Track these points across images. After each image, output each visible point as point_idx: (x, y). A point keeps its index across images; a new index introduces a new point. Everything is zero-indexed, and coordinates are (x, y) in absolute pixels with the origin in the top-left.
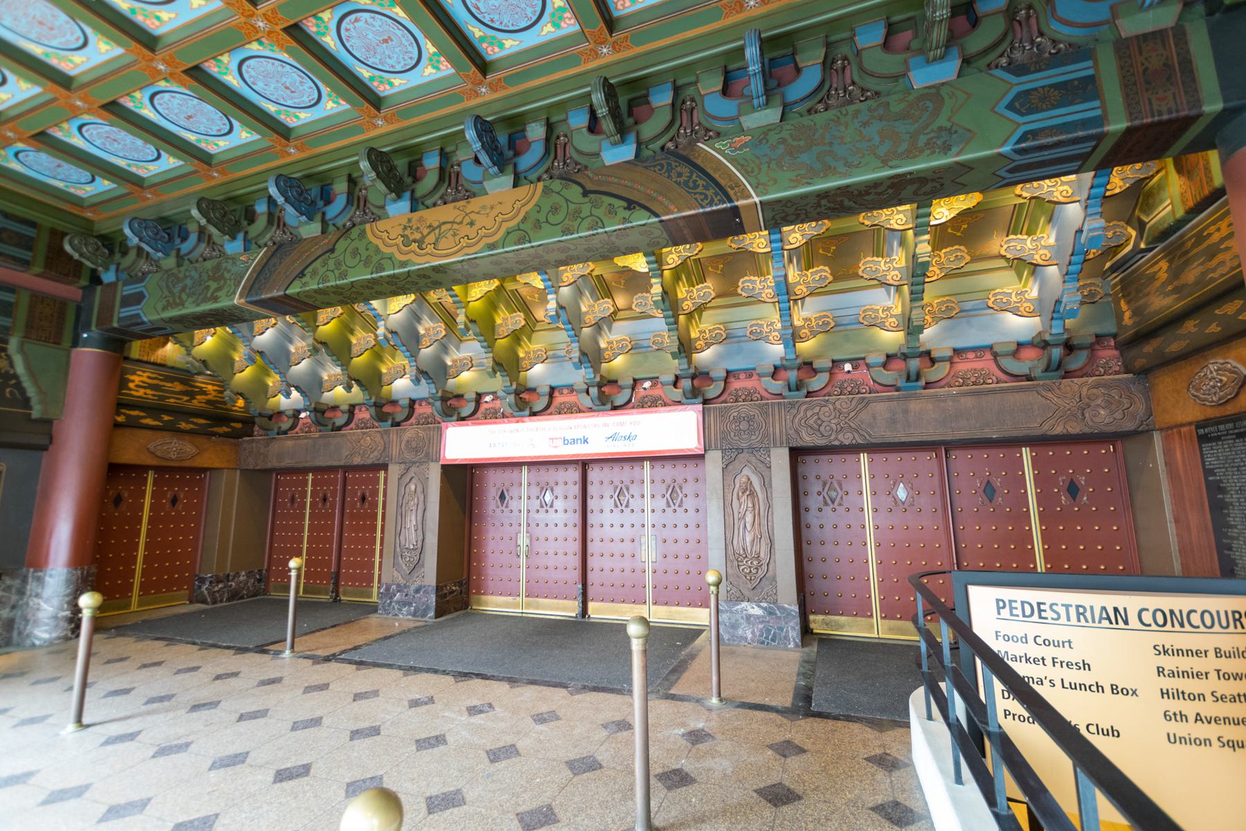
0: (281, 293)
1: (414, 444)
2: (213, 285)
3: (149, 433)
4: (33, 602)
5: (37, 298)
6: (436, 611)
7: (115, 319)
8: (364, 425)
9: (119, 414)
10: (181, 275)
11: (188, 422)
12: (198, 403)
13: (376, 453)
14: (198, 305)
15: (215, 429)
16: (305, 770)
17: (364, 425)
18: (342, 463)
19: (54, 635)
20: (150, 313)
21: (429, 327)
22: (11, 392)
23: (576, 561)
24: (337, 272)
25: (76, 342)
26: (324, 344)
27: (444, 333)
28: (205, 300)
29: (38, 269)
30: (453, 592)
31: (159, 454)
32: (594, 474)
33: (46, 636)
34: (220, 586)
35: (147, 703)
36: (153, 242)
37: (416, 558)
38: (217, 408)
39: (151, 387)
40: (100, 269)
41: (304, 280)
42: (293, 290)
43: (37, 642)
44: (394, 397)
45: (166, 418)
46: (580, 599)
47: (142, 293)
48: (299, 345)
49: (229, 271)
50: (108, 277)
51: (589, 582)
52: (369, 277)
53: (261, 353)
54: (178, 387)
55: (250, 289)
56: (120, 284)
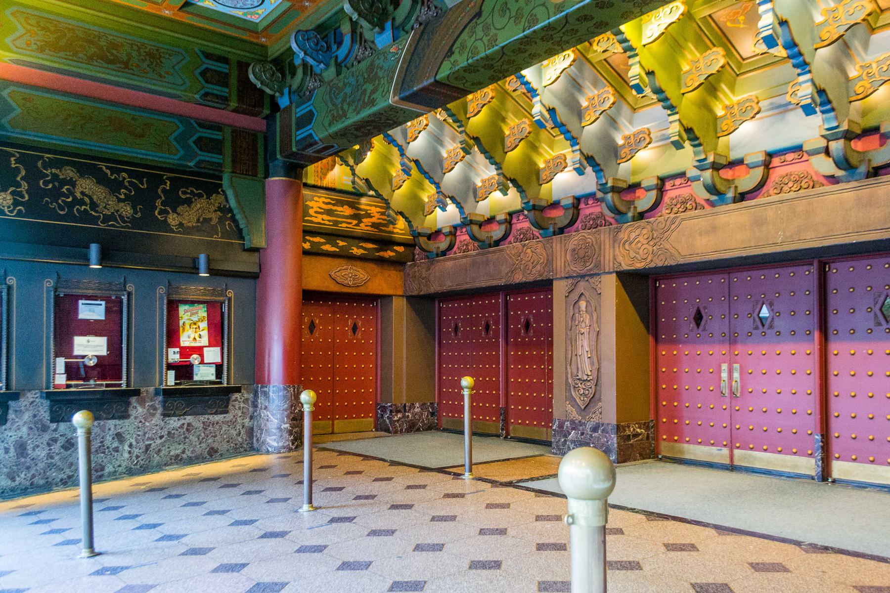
0: (432, 80)
1: (582, 253)
2: (369, 87)
3: (329, 260)
4: (264, 413)
5: (238, 133)
6: (619, 454)
7: (294, 144)
8: (525, 236)
9: (305, 241)
10: (341, 85)
12: (364, 227)
13: (538, 267)
14: (358, 113)
15: (381, 254)
16: (497, 565)
17: (525, 236)
18: (502, 282)
19: (281, 444)
20: (319, 131)
21: (596, 96)
23: (811, 405)
24: (485, 39)
25: (267, 176)
26: (476, 139)
27: (612, 100)
28: (365, 105)
29: (234, 104)
30: (636, 435)
31: (338, 280)
32: (838, 272)
33: (275, 444)
34: (399, 415)
35: (354, 499)
36: (314, 55)
37: (592, 391)
38: (381, 231)
39: (329, 212)
40: (277, 94)
41: (452, 59)
42: (444, 73)
43: (270, 449)
44: (555, 198)
45: (341, 243)
46: (819, 454)
47: (311, 111)
48: (450, 147)
49: (381, 68)
50: (284, 102)
51: (815, 296)
52: (521, 35)
53: (416, 162)
54: (347, 211)
55: (403, 83)
56: (294, 105)
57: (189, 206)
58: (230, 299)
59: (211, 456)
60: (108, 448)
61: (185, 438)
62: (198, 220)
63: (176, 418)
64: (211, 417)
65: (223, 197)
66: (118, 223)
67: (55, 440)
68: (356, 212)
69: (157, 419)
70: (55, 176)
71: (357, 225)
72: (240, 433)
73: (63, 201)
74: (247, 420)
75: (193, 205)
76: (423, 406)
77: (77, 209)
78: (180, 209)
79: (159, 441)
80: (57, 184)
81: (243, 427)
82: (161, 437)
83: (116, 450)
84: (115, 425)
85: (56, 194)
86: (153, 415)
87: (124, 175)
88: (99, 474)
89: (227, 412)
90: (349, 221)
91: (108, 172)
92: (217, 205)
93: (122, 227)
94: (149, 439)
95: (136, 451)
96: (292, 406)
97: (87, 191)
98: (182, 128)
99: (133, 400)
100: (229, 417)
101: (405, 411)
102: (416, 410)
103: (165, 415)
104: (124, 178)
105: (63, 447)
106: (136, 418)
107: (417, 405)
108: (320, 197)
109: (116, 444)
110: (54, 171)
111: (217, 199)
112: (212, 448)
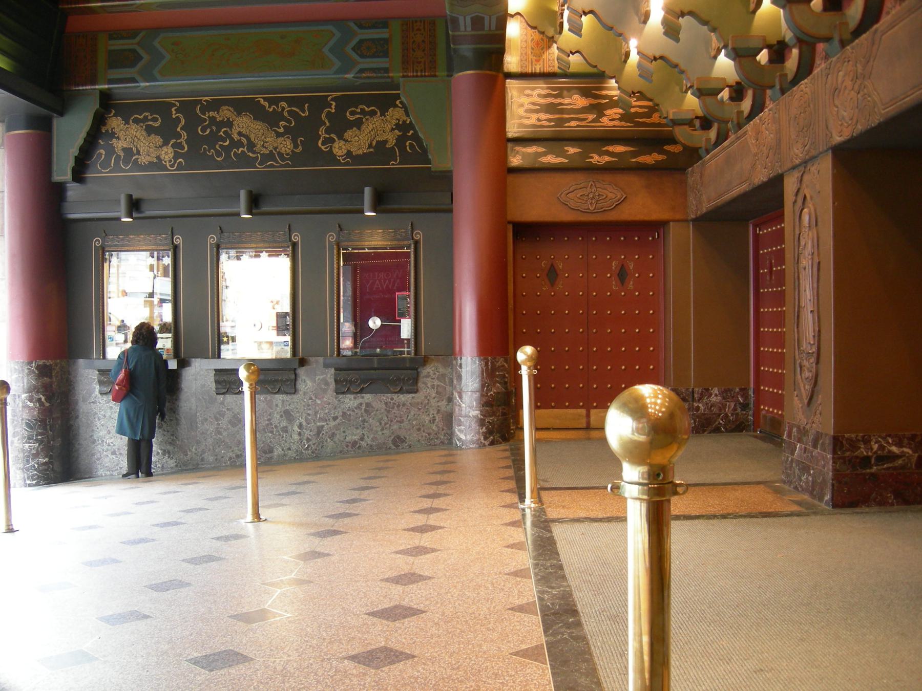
3: (558, 178)
11: (601, 154)
12: (611, 119)
22: (411, 145)
25: (450, 71)
31: (572, 204)
45: (572, 150)
54: (579, 101)
57: (359, 129)
58: (417, 243)
59: (397, 446)
60: (276, 426)
61: (364, 421)
62: (370, 146)
63: (352, 396)
64: (395, 396)
65: (402, 111)
66: (277, 162)
67: (223, 415)
68: (594, 101)
69: (330, 394)
70: (213, 119)
71: (593, 121)
72: (434, 420)
73: (221, 146)
74: (444, 402)
75: (363, 127)
76: (726, 393)
77: (235, 153)
78: (348, 134)
79: (332, 423)
80: (214, 128)
81: (439, 411)
82: (335, 418)
83: (285, 429)
84: (283, 401)
85: (213, 139)
86: (325, 391)
87: (284, 104)
88: (268, 456)
89: (416, 392)
90: (582, 116)
91: (266, 104)
92: (394, 122)
93: (282, 166)
94: (321, 419)
95: (307, 433)
96: (483, 386)
97: (244, 131)
98: (338, 35)
99: (302, 372)
100: (419, 397)
101: (694, 400)
102: (714, 399)
103: (338, 392)
104: (283, 108)
105: (230, 422)
106: (305, 394)
107: (716, 391)
108: (533, 89)
109: (284, 424)
110: (212, 114)
111: (395, 114)
112: (399, 437)
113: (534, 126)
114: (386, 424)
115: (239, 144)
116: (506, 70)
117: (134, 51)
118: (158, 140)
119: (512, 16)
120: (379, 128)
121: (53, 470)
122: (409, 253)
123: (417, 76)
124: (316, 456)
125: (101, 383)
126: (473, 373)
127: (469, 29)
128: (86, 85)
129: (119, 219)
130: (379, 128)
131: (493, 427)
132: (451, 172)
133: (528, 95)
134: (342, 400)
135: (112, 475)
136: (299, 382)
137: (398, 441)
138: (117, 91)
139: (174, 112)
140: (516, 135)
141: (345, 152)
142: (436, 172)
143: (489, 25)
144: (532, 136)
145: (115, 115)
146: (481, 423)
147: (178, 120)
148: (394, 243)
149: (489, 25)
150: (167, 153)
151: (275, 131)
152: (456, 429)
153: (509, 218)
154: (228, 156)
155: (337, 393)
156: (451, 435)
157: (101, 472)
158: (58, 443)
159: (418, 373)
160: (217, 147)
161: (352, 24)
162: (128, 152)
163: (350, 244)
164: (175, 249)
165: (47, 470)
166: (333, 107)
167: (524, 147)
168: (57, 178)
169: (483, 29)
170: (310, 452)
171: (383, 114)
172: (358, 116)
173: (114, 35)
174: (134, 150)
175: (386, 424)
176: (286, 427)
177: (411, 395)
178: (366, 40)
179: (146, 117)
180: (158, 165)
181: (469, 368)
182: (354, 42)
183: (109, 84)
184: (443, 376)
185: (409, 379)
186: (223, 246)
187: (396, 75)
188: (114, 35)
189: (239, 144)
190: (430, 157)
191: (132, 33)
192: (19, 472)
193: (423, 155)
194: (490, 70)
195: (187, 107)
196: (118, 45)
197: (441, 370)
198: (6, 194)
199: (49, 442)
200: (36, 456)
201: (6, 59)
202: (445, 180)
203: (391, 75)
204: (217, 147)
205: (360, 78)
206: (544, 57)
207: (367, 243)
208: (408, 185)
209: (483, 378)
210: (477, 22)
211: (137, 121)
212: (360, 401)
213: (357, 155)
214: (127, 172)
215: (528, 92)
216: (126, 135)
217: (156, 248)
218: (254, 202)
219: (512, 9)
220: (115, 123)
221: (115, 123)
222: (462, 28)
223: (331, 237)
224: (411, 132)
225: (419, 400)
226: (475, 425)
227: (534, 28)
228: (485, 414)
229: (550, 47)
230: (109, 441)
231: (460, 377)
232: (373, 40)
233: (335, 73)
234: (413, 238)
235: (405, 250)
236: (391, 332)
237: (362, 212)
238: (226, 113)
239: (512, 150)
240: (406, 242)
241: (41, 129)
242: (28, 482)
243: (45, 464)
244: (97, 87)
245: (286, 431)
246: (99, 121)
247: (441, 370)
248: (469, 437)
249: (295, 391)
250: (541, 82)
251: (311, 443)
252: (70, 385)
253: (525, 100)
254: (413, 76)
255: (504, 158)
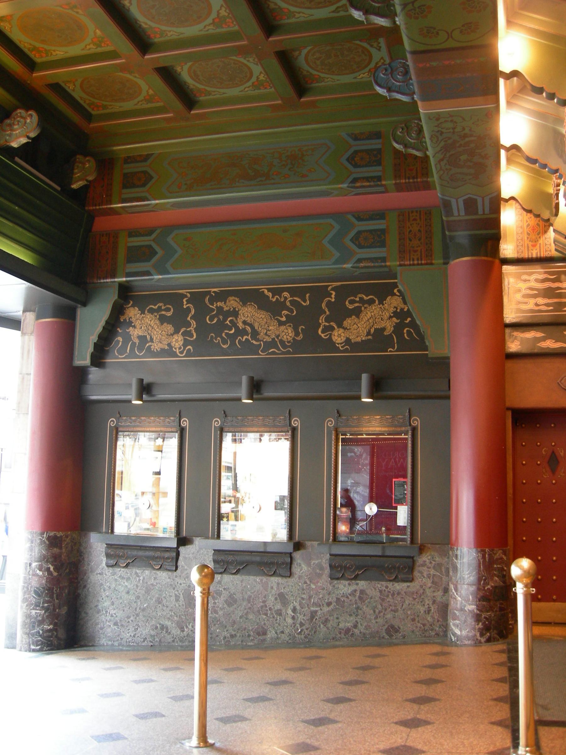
22: (409, 333)
25: (447, 259)
57: (358, 317)
58: (414, 430)
59: (391, 636)
60: (270, 609)
61: (358, 608)
62: (368, 333)
63: (347, 583)
64: (390, 585)
65: (400, 299)
66: (279, 350)
70: (220, 309)
72: (429, 611)
73: (227, 334)
74: (440, 593)
75: (362, 315)
78: (347, 322)
79: (326, 609)
80: (221, 317)
81: (434, 602)
82: (329, 604)
83: (279, 612)
84: (278, 584)
85: (221, 326)
86: (320, 576)
87: (286, 294)
89: (412, 580)
91: (270, 295)
92: (392, 310)
93: (283, 353)
94: (315, 604)
95: (300, 618)
96: (479, 579)
98: (337, 227)
99: (297, 555)
100: (414, 586)
103: (332, 578)
104: (286, 298)
105: (226, 601)
106: (300, 577)
108: (531, 274)
109: (278, 606)
110: (219, 304)
111: (393, 303)
112: (392, 627)
113: (532, 311)
114: (380, 612)
115: (244, 332)
116: (502, 256)
117: (150, 247)
118: (170, 328)
119: (506, 201)
120: (376, 317)
121: (56, 636)
122: (406, 439)
123: (414, 265)
124: (308, 643)
125: (108, 556)
126: (469, 565)
127: (462, 213)
128: (106, 278)
129: (130, 401)
130: (376, 317)
131: (490, 623)
132: (448, 358)
133: (525, 281)
134: (337, 586)
135: (113, 645)
136: (294, 566)
137: (392, 630)
138: (137, 283)
139: (185, 303)
140: (514, 321)
141: (344, 339)
142: (432, 358)
143: (483, 208)
144: (530, 321)
145: (133, 306)
146: (478, 618)
147: (188, 309)
148: (391, 429)
149: (483, 208)
150: (178, 341)
151: (277, 319)
152: (451, 623)
153: (508, 404)
154: (233, 344)
155: (332, 579)
156: (446, 628)
157: (103, 641)
158: (64, 610)
159: (414, 562)
160: (223, 335)
161: (350, 217)
162: (143, 339)
163: (348, 429)
164: (182, 431)
165: (51, 637)
166: (333, 296)
167: (523, 332)
168: (78, 362)
169: (477, 213)
170: (303, 636)
171: (381, 302)
172: (357, 305)
173: (133, 233)
174: (148, 337)
175: (380, 612)
176: (281, 610)
177: (405, 584)
178: (364, 231)
179: (160, 308)
180: (169, 352)
181: (466, 557)
182: (352, 234)
183: (126, 277)
184: (440, 565)
185: (405, 567)
186: (226, 429)
187: (393, 263)
188: (133, 233)
189: (244, 332)
190: (427, 344)
191: (149, 232)
192: (25, 636)
193: (420, 342)
194: (487, 256)
195: (197, 299)
196: (136, 241)
197: (437, 559)
198: (32, 377)
199: (54, 610)
200: (41, 622)
201: (30, 253)
202: (442, 366)
203: (388, 264)
204: (223, 335)
205: (358, 267)
206: (541, 241)
207: (364, 429)
208: (405, 373)
209: (479, 570)
210: (470, 205)
211: (151, 311)
212: (354, 587)
213: (356, 343)
214: (142, 358)
215: (525, 277)
216: (142, 324)
217: (162, 429)
218: (255, 387)
219: (505, 194)
220: (132, 313)
221: (132, 313)
222: (455, 213)
223: (330, 423)
224: (409, 319)
225: (414, 590)
226: (471, 621)
227: (529, 211)
228: (481, 609)
229: (546, 232)
230: (112, 612)
231: (455, 569)
232: (370, 231)
233: (334, 264)
234: (410, 425)
235: (403, 436)
236: (386, 518)
237: (359, 398)
238: (232, 303)
239: (510, 336)
240: (403, 429)
241: (65, 319)
242: (33, 647)
243: (50, 630)
244: (116, 280)
245: (280, 614)
246: (118, 311)
247: (437, 559)
248: (464, 633)
249: (291, 575)
250: (537, 267)
251: (304, 627)
252: (81, 556)
253: (522, 286)
254: (410, 265)
255: (502, 342)
